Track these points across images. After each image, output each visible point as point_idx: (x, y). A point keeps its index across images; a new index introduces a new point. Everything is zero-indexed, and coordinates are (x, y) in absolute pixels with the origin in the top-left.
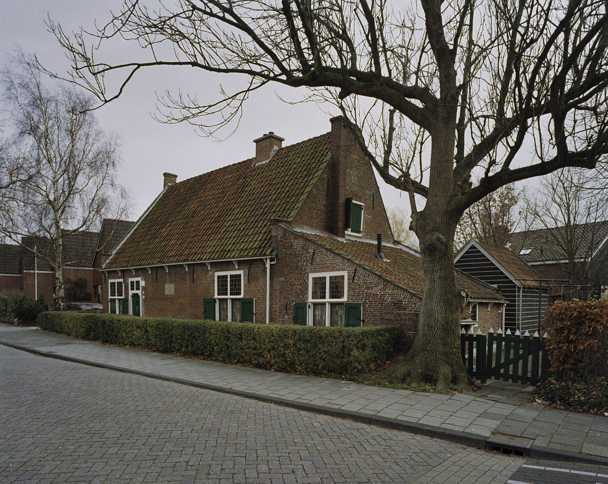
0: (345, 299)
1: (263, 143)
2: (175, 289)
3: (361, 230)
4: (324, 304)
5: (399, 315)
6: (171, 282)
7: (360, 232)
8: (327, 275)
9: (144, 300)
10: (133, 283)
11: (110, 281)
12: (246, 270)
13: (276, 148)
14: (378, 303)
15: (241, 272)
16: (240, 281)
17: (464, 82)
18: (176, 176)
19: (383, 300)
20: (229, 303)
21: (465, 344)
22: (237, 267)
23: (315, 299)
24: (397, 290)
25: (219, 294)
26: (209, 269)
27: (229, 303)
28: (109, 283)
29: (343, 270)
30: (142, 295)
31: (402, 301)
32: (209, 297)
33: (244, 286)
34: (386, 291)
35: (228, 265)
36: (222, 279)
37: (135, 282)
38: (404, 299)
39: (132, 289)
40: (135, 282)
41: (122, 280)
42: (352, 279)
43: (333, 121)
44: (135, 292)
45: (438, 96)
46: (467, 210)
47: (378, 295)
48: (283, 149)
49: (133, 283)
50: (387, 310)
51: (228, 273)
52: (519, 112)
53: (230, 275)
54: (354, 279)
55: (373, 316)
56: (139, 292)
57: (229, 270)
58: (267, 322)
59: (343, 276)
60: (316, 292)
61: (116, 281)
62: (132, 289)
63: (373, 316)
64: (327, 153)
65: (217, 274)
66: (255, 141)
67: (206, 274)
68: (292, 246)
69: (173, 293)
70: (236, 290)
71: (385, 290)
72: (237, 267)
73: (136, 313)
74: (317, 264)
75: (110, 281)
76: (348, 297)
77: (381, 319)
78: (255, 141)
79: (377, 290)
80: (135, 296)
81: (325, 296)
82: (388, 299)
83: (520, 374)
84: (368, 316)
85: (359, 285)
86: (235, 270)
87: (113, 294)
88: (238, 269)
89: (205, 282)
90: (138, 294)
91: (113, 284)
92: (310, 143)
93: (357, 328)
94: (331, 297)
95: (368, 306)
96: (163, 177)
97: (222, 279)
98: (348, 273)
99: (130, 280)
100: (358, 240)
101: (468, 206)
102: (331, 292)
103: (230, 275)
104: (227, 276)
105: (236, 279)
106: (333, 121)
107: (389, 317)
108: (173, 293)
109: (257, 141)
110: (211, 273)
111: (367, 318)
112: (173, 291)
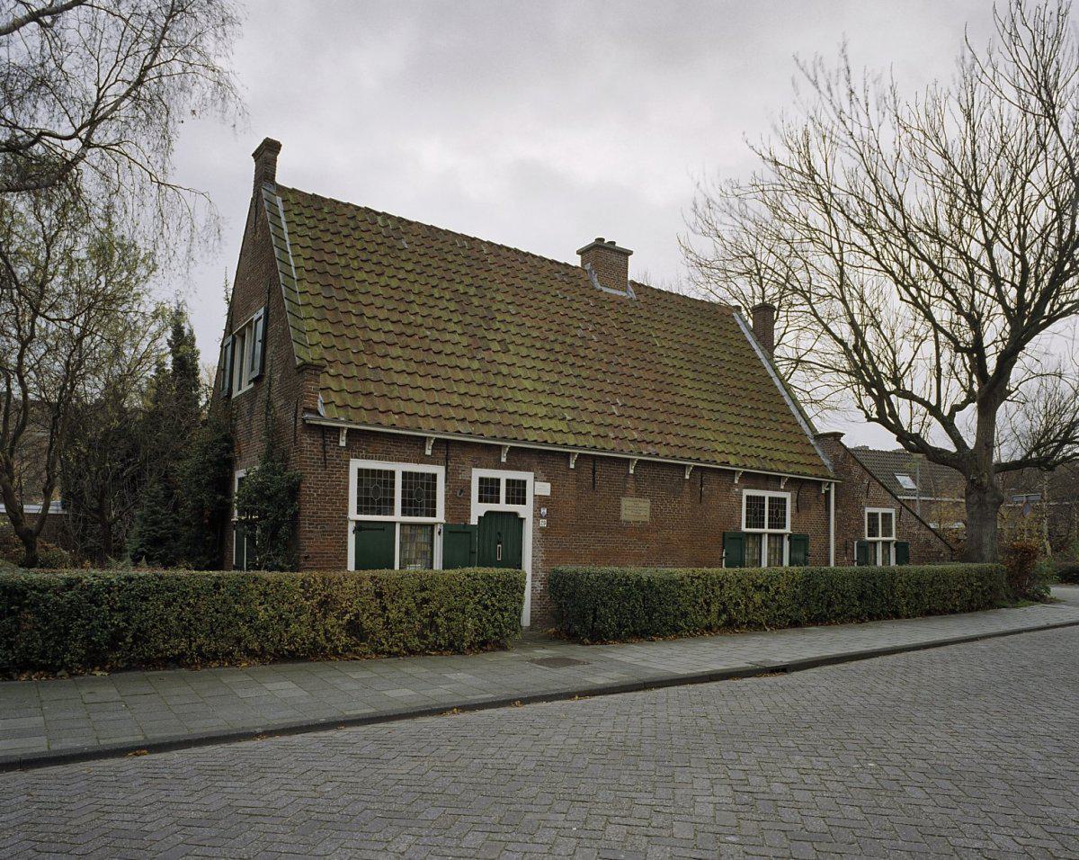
0: (893, 538)
2: (652, 510)
4: (760, 535)
5: (929, 553)
6: (640, 494)
8: (880, 511)
9: (543, 535)
11: (868, 510)
15: (787, 496)
17: (627, 259)
18: (604, 240)
20: (880, 548)
23: (410, 515)
25: (360, 511)
27: (880, 548)
28: (866, 515)
29: (892, 507)
30: (537, 516)
32: (731, 529)
35: (409, 445)
37: (767, 500)
40: (767, 500)
42: (899, 515)
44: (502, 506)
51: (767, 494)
53: (770, 498)
56: (525, 511)
57: (768, 489)
58: (351, 566)
59: (891, 514)
61: (880, 511)
65: (747, 492)
66: (578, 253)
67: (728, 491)
68: (850, 472)
69: (549, 494)
70: (777, 521)
72: (782, 487)
73: (886, 560)
75: (868, 510)
78: (578, 253)
79: (915, 530)
81: (763, 524)
87: (873, 533)
88: (785, 490)
89: (725, 503)
92: (658, 296)
93: (385, 571)
94: (404, 513)
103: (770, 498)
105: (778, 504)
108: (549, 494)
110: (737, 490)
112: (648, 514)
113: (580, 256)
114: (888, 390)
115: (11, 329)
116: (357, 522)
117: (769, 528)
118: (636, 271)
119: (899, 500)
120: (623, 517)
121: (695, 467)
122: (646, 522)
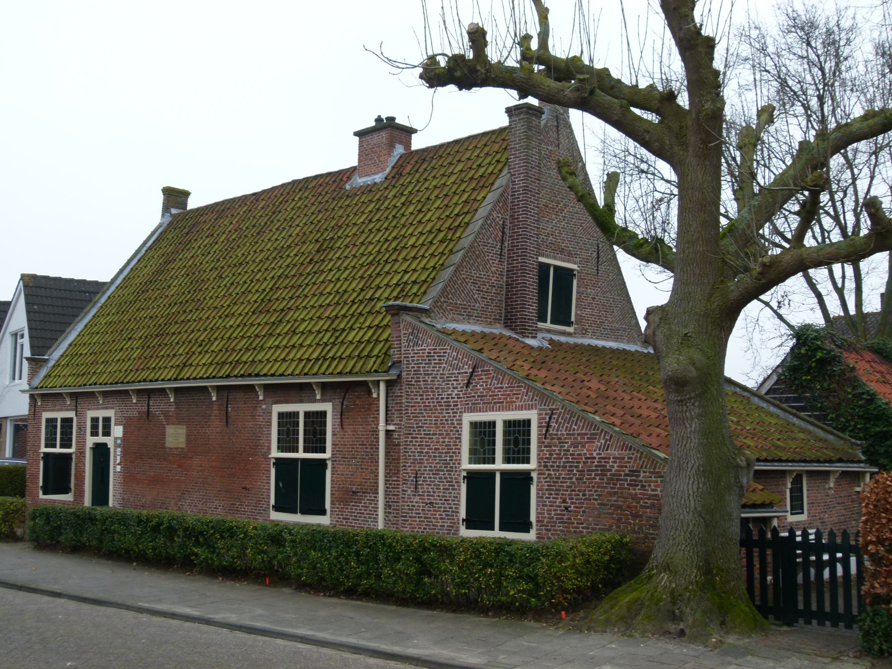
1: (376, 138)
2: (188, 435)
3: (573, 319)
7: (569, 323)
8: (499, 417)
10: (95, 420)
11: (46, 415)
12: (338, 402)
13: (399, 150)
14: (596, 475)
15: (327, 407)
16: (324, 424)
18: (186, 194)
19: (605, 470)
21: (752, 552)
22: (318, 397)
24: (625, 451)
26: (261, 398)
29: (530, 408)
31: (639, 472)
33: (334, 435)
34: (609, 451)
35: (301, 391)
36: (288, 420)
38: (642, 467)
39: (94, 433)
41: (71, 414)
43: (509, 111)
44: (101, 439)
45: (615, 248)
46: (855, 145)
47: (595, 458)
48: (412, 152)
49: (95, 420)
50: (611, 488)
51: (301, 408)
52: (763, 241)
54: (548, 426)
55: (585, 499)
56: (109, 441)
57: (301, 401)
59: (529, 421)
60: (475, 449)
61: (59, 415)
62: (94, 433)
63: (585, 499)
64: (501, 171)
66: (357, 134)
67: (255, 408)
69: (183, 445)
71: (607, 450)
72: (318, 397)
73: (100, 494)
74: (478, 396)
75: (46, 415)
76: (539, 462)
77: (599, 504)
78: (357, 134)
80: (101, 451)
81: (298, 447)
82: (613, 467)
83: (827, 608)
84: (577, 499)
85: (559, 439)
86: (314, 401)
88: (323, 400)
90: (105, 445)
91: (51, 422)
94: (507, 460)
95: (577, 479)
96: (160, 197)
97: (288, 420)
98: (539, 414)
99: (91, 414)
100: (563, 339)
101: (858, 140)
102: (506, 451)
104: (298, 413)
105: (316, 420)
106: (509, 111)
107: (615, 501)
108: (183, 445)
109: (359, 134)
110: (264, 407)
111: (575, 503)
113: (357, 139)
114: (835, 125)
115: (690, 622)
116: (277, 459)
117: (305, 452)
118: (397, 121)
119: (289, 375)
120: (168, 445)
121: (843, 472)
122: (183, 449)
